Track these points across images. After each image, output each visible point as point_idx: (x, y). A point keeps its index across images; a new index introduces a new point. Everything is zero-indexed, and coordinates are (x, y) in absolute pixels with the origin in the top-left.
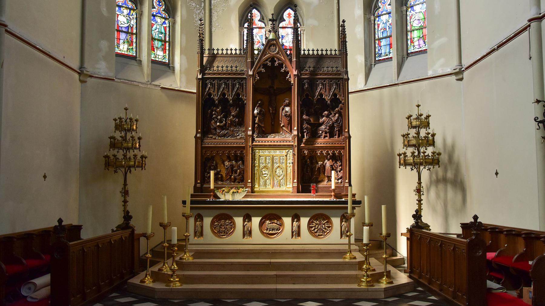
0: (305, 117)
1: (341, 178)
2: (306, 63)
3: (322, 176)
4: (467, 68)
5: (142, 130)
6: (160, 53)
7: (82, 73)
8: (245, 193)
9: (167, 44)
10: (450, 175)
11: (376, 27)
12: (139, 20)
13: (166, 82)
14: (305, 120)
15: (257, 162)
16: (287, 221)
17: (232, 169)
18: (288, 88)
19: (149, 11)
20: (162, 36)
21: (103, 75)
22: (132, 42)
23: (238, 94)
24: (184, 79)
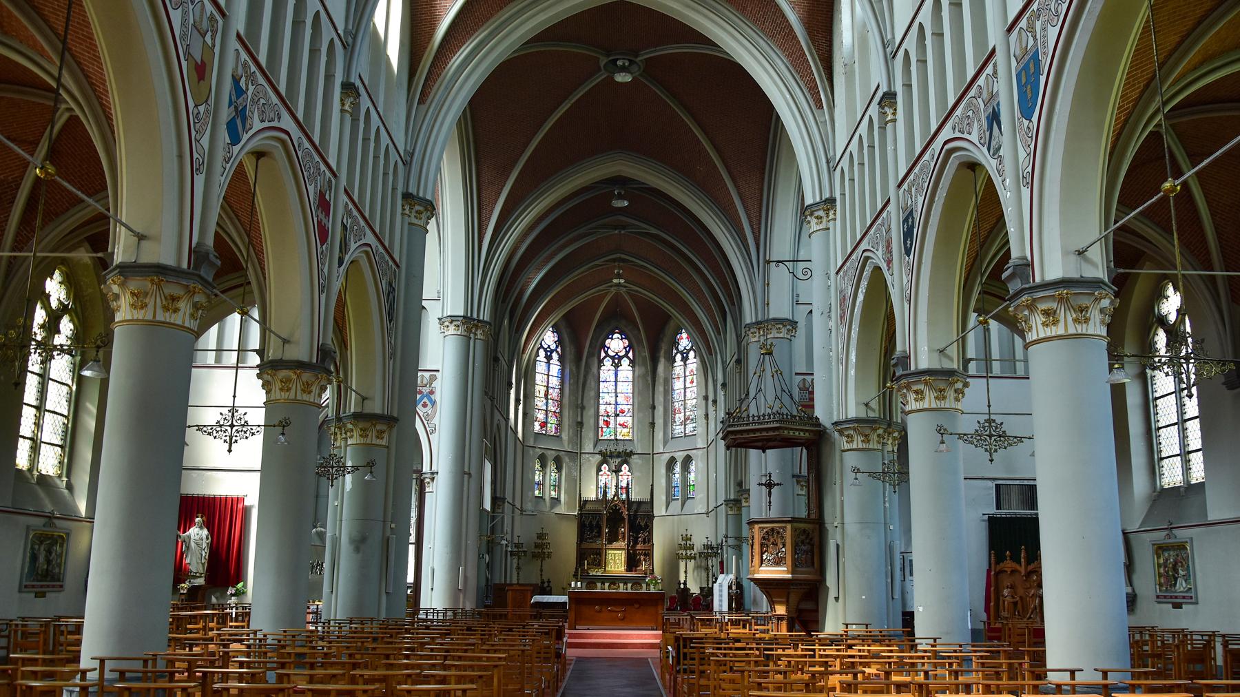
13: (557, 510)
17: (594, 560)
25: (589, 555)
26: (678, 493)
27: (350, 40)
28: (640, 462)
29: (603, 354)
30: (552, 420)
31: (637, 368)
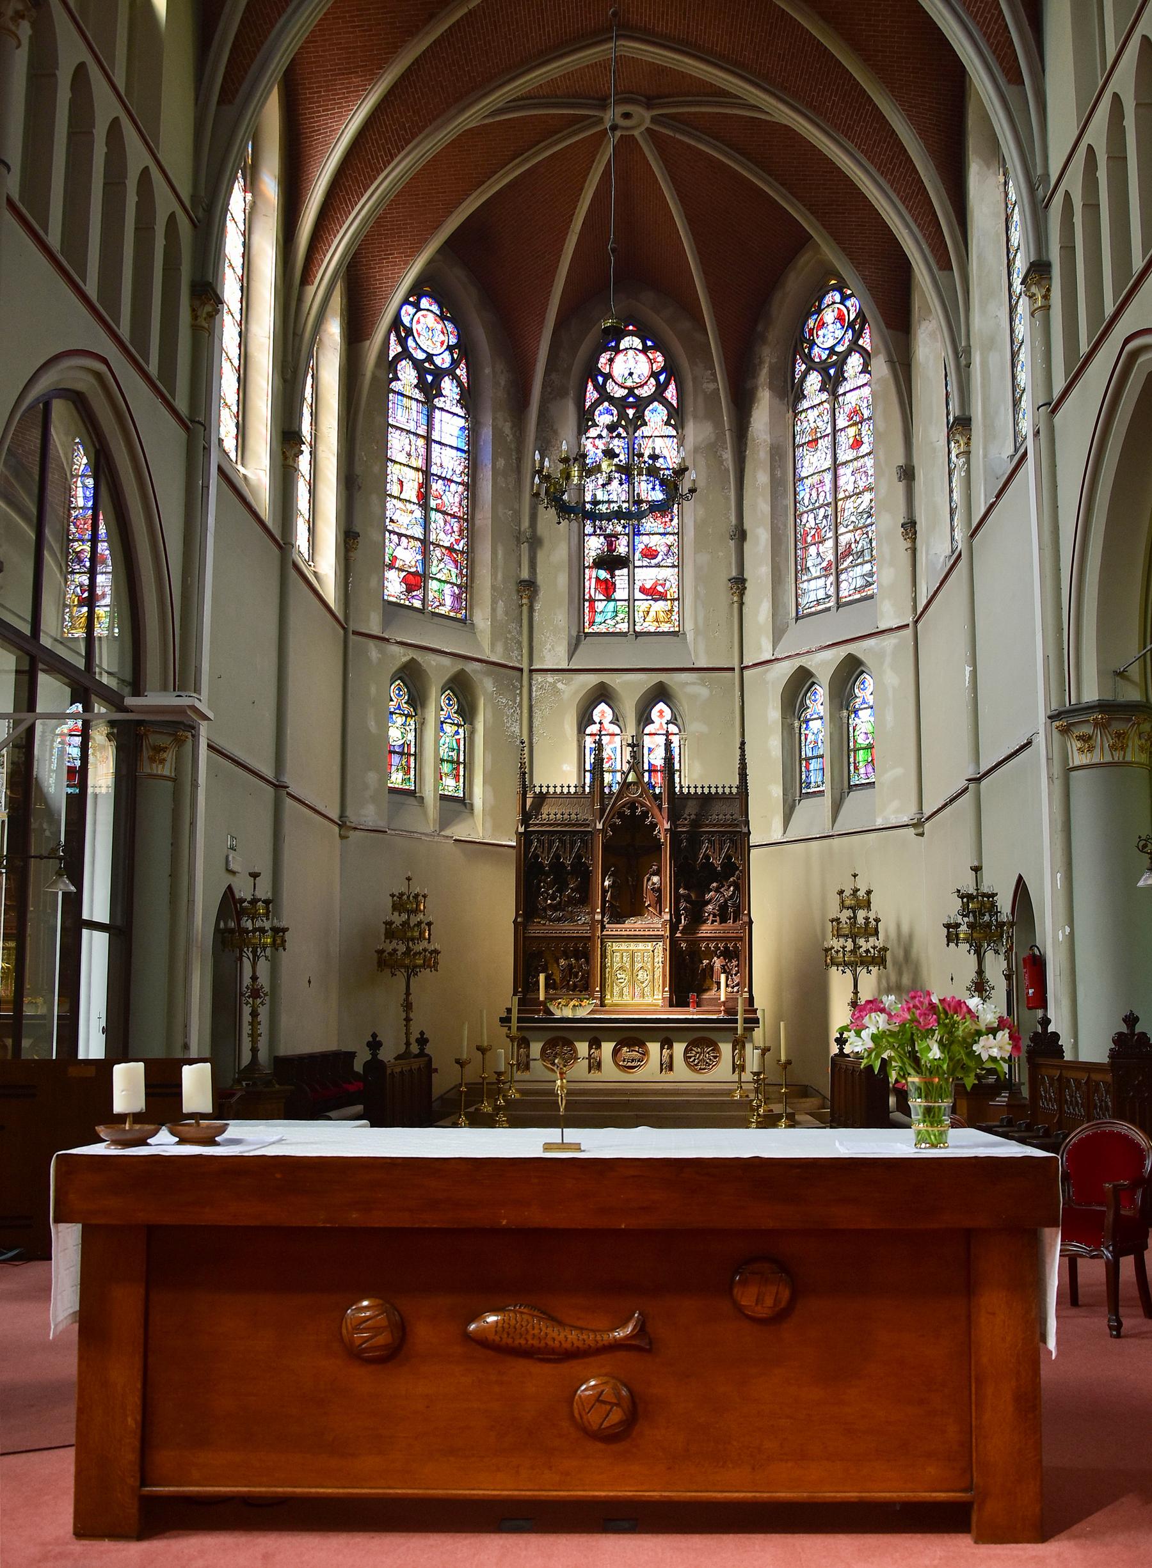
0: (681, 891)
1: (737, 985)
2: (685, 807)
3: (708, 981)
4: (927, 819)
5: (431, 911)
6: (450, 782)
7: (343, 824)
8: (592, 1007)
9: (462, 766)
10: (906, 980)
11: (803, 738)
12: (419, 732)
13: (460, 831)
14: (683, 895)
15: (608, 960)
16: (654, 1048)
17: (570, 971)
18: (657, 846)
19: (437, 715)
20: (454, 754)
21: (371, 824)
22: (409, 768)
23: (579, 857)
24: (489, 825)
25: (554, 958)
26: (818, 775)
27: (201, 214)
28: (704, 692)
29: (591, 394)
30: (444, 569)
31: (690, 428)
